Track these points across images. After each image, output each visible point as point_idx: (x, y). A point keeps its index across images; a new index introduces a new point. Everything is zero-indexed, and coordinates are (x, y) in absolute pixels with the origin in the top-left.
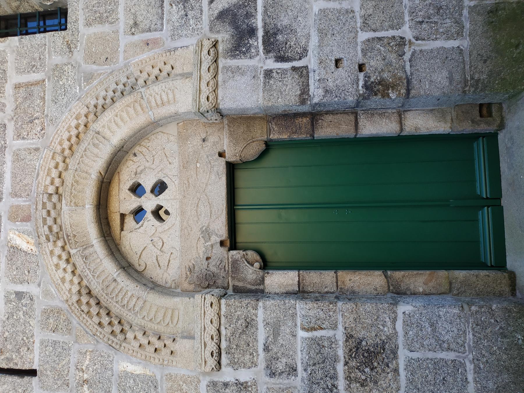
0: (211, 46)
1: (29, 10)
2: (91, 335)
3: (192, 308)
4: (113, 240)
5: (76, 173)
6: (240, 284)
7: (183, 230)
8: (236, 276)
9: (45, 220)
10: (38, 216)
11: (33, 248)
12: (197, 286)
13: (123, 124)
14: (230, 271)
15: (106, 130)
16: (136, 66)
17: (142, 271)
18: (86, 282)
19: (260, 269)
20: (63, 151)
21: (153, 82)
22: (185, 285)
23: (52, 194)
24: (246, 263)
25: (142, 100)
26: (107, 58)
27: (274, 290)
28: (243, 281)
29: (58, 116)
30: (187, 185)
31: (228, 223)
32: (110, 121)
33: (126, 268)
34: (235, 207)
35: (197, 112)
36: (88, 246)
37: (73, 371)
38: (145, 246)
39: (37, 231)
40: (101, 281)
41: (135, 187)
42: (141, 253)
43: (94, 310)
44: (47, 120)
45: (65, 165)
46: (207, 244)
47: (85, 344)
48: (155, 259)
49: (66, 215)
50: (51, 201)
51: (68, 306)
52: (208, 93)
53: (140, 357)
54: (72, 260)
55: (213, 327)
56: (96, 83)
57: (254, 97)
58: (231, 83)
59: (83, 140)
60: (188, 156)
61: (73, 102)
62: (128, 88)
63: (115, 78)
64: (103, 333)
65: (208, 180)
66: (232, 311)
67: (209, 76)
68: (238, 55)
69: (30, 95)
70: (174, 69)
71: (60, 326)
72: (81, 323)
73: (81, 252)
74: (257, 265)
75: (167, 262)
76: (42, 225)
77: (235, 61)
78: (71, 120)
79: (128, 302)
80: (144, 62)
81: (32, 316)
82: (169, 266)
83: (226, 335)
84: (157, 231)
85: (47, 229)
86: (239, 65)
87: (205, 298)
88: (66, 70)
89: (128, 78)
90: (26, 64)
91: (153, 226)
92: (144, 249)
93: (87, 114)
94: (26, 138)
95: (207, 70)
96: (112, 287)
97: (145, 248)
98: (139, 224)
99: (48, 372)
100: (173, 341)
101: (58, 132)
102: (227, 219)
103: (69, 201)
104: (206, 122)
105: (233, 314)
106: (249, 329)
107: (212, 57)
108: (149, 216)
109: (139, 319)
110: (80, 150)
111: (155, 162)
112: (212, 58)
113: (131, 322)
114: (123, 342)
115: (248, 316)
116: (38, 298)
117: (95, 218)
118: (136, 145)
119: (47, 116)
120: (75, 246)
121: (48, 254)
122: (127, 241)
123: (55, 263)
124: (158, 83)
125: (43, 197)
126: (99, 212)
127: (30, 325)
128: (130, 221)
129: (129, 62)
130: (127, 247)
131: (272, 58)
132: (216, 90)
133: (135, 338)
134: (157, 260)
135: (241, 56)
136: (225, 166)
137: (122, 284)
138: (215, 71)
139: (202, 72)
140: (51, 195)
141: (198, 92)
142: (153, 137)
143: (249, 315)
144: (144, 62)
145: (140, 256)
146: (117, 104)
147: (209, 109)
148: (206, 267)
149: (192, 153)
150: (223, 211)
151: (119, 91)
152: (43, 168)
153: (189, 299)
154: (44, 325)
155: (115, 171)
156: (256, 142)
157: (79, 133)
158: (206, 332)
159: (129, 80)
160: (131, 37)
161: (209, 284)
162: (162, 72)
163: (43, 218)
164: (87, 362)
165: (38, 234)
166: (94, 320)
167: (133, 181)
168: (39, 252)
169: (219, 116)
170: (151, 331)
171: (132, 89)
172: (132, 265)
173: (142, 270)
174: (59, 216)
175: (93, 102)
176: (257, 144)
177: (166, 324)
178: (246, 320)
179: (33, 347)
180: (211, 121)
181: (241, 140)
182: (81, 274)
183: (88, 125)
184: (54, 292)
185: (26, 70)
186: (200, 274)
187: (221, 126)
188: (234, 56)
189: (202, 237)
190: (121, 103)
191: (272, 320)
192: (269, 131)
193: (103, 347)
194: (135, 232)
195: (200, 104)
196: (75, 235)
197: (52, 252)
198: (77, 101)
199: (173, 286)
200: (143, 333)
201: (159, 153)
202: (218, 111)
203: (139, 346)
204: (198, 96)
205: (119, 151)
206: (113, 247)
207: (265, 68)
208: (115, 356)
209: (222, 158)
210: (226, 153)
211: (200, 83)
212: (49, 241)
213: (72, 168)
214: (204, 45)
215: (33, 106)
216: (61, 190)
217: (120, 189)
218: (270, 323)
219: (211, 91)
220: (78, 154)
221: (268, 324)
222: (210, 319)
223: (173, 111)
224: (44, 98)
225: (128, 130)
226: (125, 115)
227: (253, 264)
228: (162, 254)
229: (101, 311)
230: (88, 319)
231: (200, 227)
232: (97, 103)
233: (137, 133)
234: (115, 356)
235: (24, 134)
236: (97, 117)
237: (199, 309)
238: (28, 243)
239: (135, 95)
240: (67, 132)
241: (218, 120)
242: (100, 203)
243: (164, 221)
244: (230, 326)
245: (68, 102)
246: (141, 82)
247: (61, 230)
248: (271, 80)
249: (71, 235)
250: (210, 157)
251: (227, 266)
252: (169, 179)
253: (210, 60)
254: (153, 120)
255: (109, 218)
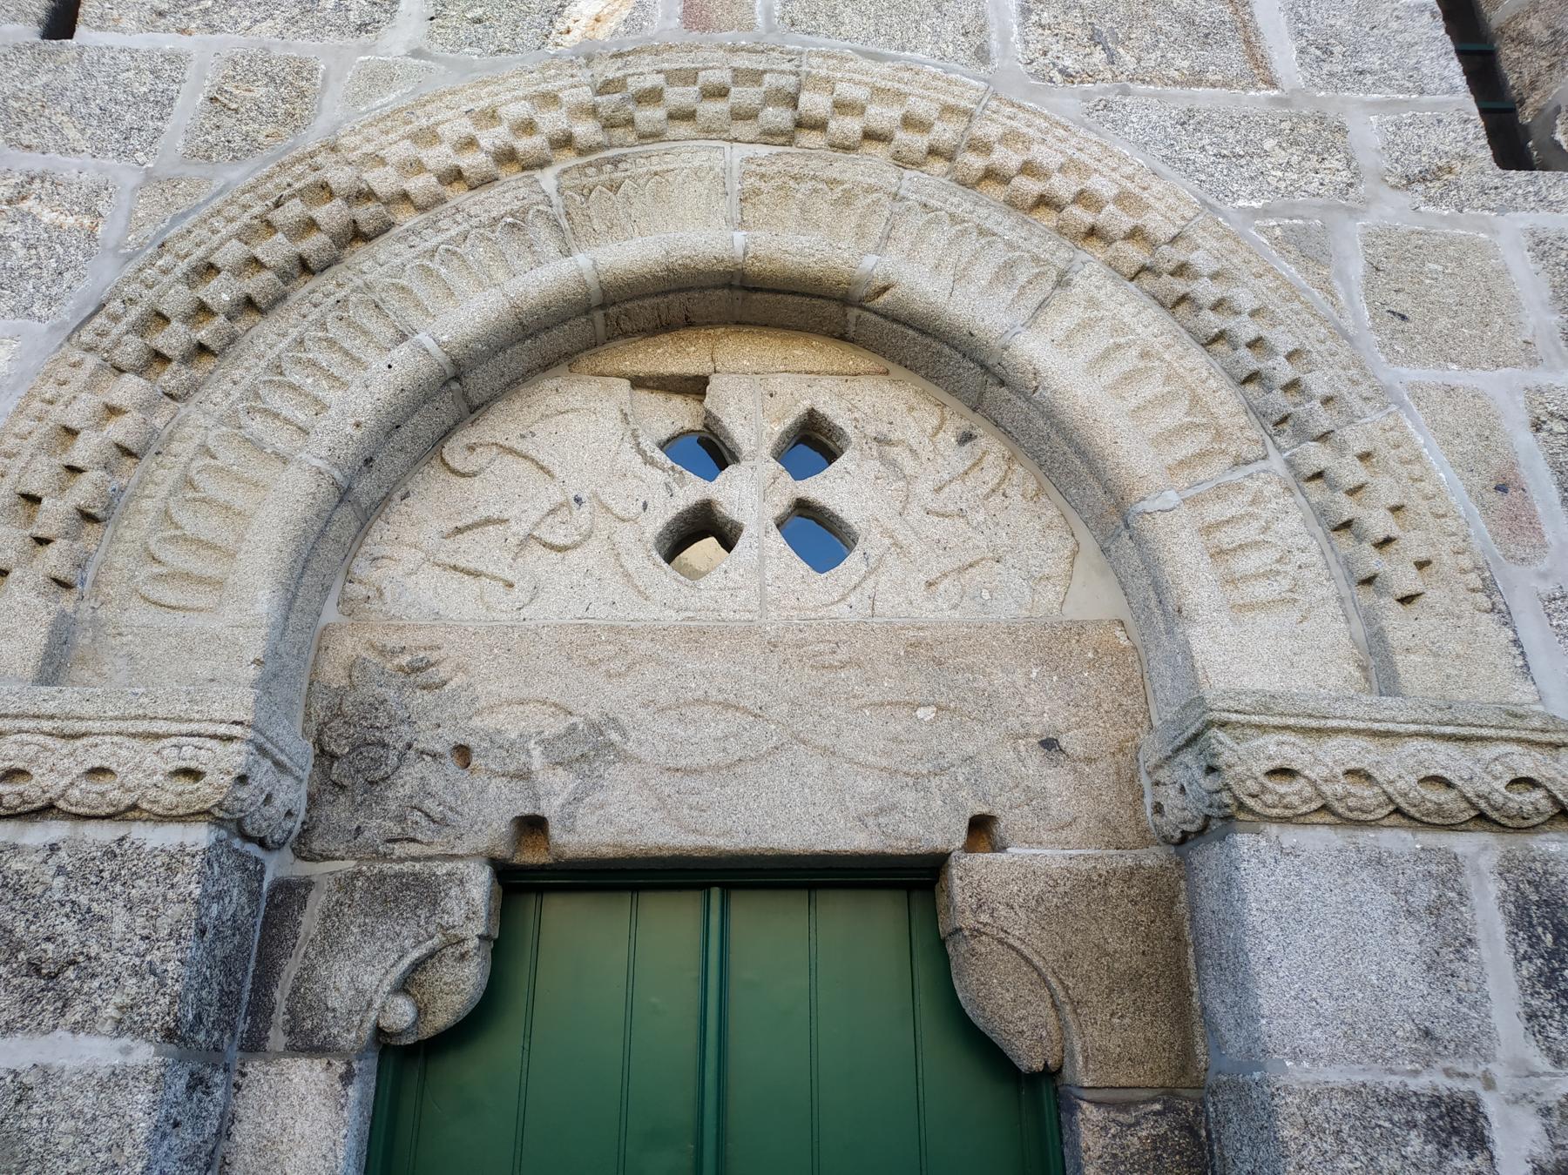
0: (1561, 797)
1: (1516, 75)
2: (164, 231)
3: (207, 674)
4: (592, 345)
5: (886, 200)
6: (309, 921)
7: (612, 637)
8: (357, 896)
9: (689, 77)
10: (706, 55)
11: (576, 34)
12: (337, 700)
13: (1106, 379)
14: (386, 867)
15: (1078, 313)
16: (1388, 434)
17: (443, 460)
18: (410, 223)
19: (379, 1031)
20: (980, 146)
21: (1321, 513)
22: (349, 642)
23: (796, 107)
24: (415, 954)
25: (1229, 460)
26: (1403, 318)
27: (250, 1113)
28: (326, 934)
29: (1126, 129)
30: (828, 659)
31: (632, 859)
32: (1120, 328)
33: (455, 386)
34: (715, 893)
35: (1207, 717)
36: (567, 235)
37: (25, 165)
38: (557, 471)
39: (642, 51)
40: (404, 282)
41: (824, 439)
42: (525, 457)
43: (275, 250)
44: (1107, 91)
45: (918, 157)
46: (537, 752)
47: (132, 212)
48: (493, 512)
49: (704, 155)
50: (766, 102)
51: (309, 149)
52: (1313, 776)
53: (16, 430)
54: (511, 176)
55: (66, 781)
56: (1287, 271)
57: (1317, 1033)
58: (1379, 902)
59: (1027, 222)
60: (970, 668)
61: (1195, 187)
62: (1280, 401)
63: (1322, 348)
64: (166, 279)
65: (851, 761)
66: (140, 882)
67: (1400, 784)
68: (1535, 942)
69: (1206, 36)
70: (1399, 606)
71: (228, 122)
72: (227, 196)
73: (541, 207)
74: (401, 1013)
75: (472, 566)
76: (666, 66)
77: (1501, 928)
78: (1116, 176)
79: (292, 387)
80: (1417, 470)
81: (295, 29)
82: (450, 574)
83: (15, 847)
84: (620, 525)
85: (648, 85)
86: (1481, 944)
87: (230, 739)
88: (1327, 164)
89: (1327, 401)
90: (1331, 26)
91: (645, 506)
92: (542, 468)
93: (1144, 239)
94: (1026, 19)
95: (1432, 772)
96: (373, 324)
97: (548, 472)
98: (657, 450)
99: (44, 79)
100: (55, 580)
101: (1062, 131)
102: (656, 853)
103: (763, 170)
104: (1140, 756)
105: (118, 888)
106: (16, 982)
107: (1500, 800)
108: (692, 490)
109: (202, 431)
110: (983, 212)
111: (936, 519)
112: (1498, 799)
113: (199, 396)
114: (105, 360)
115: (94, 976)
116: (365, 50)
117: (686, 266)
118: (1009, 442)
119: (1125, 92)
120: (569, 188)
121: (544, 87)
122: (587, 400)
123: (502, 111)
124: (1319, 531)
125: (783, 72)
126: (716, 287)
127: (256, 21)
128: (676, 415)
129: (1401, 405)
130: (556, 401)
131: (1556, 1147)
132: (1329, 818)
133: (113, 411)
134: (488, 521)
135: (1530, 960)
136: (923, 850)
137: (378, 363)
138: (1428, 815)
139: (1416, 744)
140: (793, 101)
141: (1314, 723)
142: (1051, 513)
143: (96, 984)
144: (1417, 470)
145: (511, 451)
146: (1198, 359)
147: (1229, 776)
148: (420, 746)
149: (982, 683)
150: (695, 831)
151: (1261, 366)
152: (907, 75)
153: (257, 662)
154: (244, 69)
155: (892, 359)
156: (1052, 1020)
157: (1059, 207)
158: (49, 741)
159: (1317, 404)
160: (1525, 418)
161: (334, 757)
162: (1375, 551)
163: (696, 71)
164: (47, 216)
165: (630, 53)
166: (228, 245)
167: (849, 430)
168: (555, 56)
169: (1186, 827)
170: (134, 480)
171: (1276, 418)
172: (473, 417)
173: (447, 458)
174: (703, 131)
175: (1199, 259)
176: (1044, 1026)
177: (153, 547)
178: (73, 963)
179: (166, 30)
180: (1146, 782)
181: (1062, 938)
182: (448, 205)
183: (1095, 242)
184: (378, 103)
185: (1306, 26)
186: (391, 717)
187: (1130, 835)
188: (1521, 919)
189: (574, 727)
190: (1205, 374)
191: (35, 1123)
192: (1117, 1102)
193: (101, 275)
194: (620, 433)
195: (1248, 731)
196: (619, 187)
197: (550, 99)
198: (1200, 199)
199: (356, 590)
200: (129, 443)
201: (980, 540)
202: (1215, 825)
203: (69, 424)
204: (1291, 721)
205: (982, 366)
206: (559, 338)
207: (1491, 1105)
208: (44, 327)
209: (964, 833)
210: (990, 856)
211: (1357, 732)
212: (599, 93)
213: (905, 183)
214: (1557, 760)
215: (1162, 45)
216: (810, 139)
217: (813, 376)
218: (22, 1108)
219: (1325, 788)
220: (968, 206)
221: (23, 1094)
222: (114, 767)
223: (1189, 601)
224: (1199, 83)
225: (1082, 401)
226: (1152, 387)
227: (407, 992)
228: (513, 541)
229: (268, 275)
230: (236, 225)
231: (624, 719)
232: (1197, 276)
233: (1069, 441)
234: (44, 327)
235: (1045, 14)
236: (1132, 280)
237: (179, 708)
238: (597, 20)
239: (1248, 433)
240: (1060, 159)
241: (1158, 819)
242: (756, 290)
243: (670, 557)
244: (61, 870)
245: (1192, 167)
246: (1317, 456)
247: (643, 137)
248: (1426, 1142)
249: (618, 175)
250: (966, 770)
251: (414, 849)
252: (856, 579)
253: (1485, 789)
254: (1140, 507)
255: (689, 334)
